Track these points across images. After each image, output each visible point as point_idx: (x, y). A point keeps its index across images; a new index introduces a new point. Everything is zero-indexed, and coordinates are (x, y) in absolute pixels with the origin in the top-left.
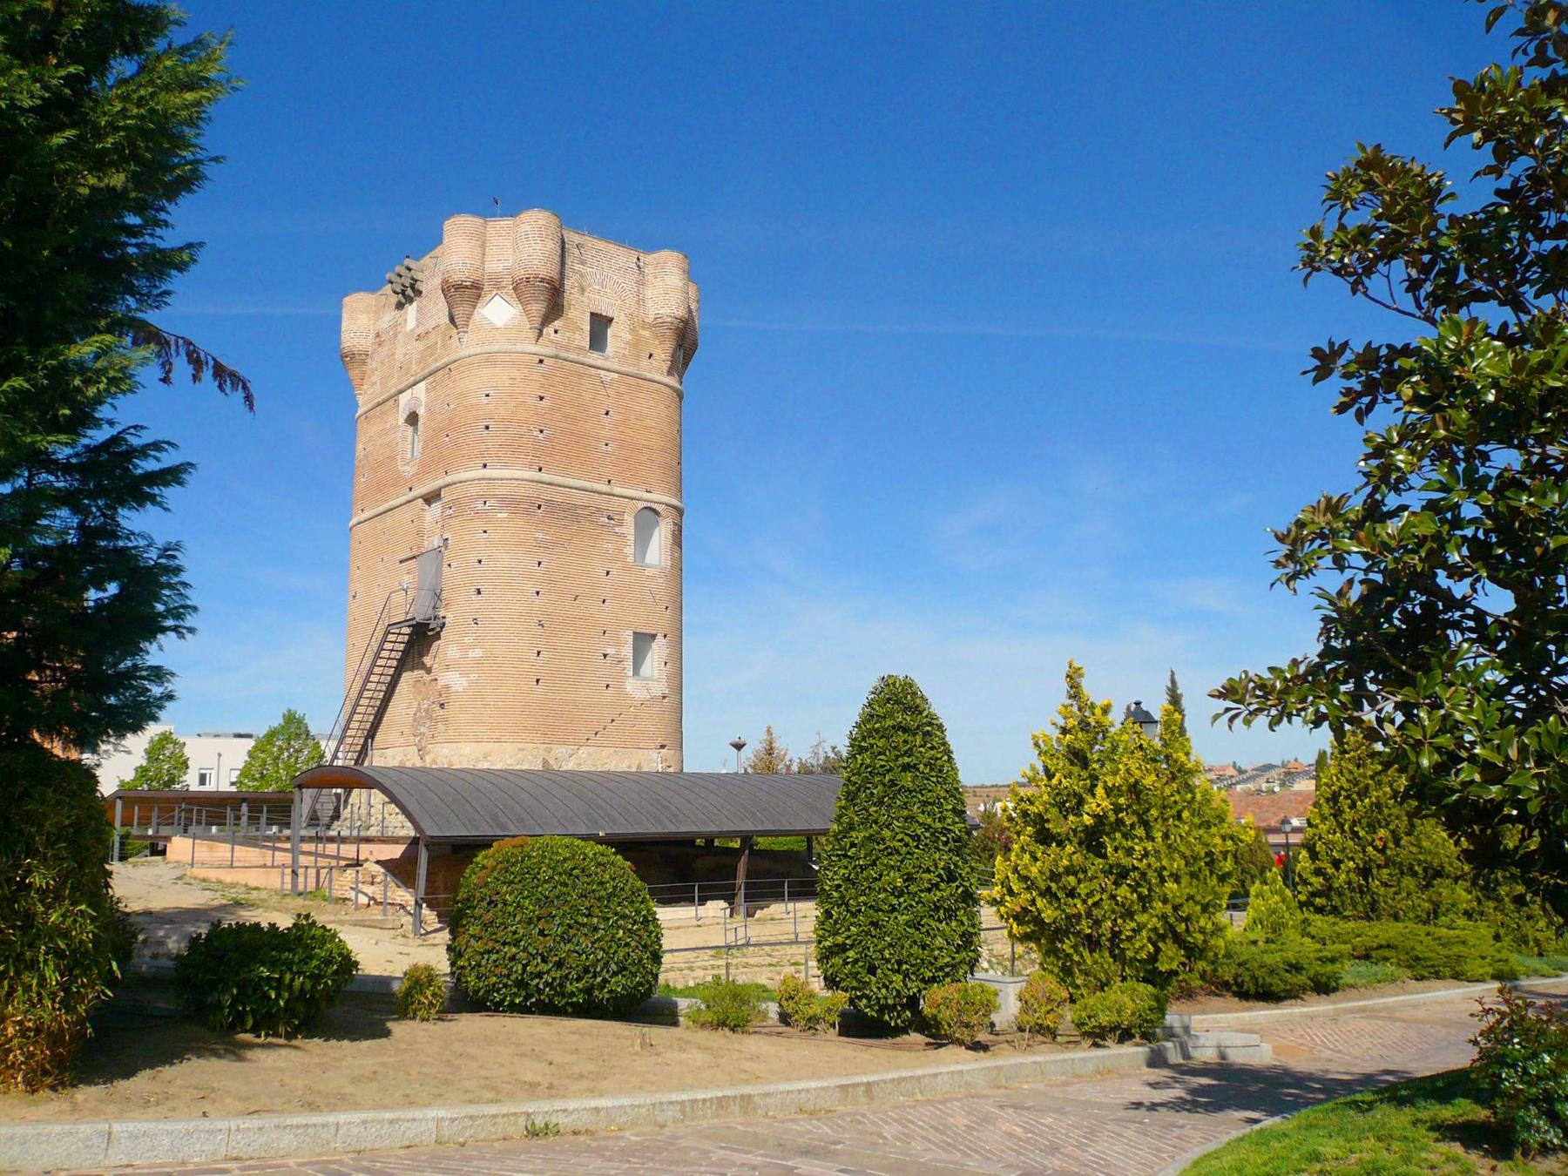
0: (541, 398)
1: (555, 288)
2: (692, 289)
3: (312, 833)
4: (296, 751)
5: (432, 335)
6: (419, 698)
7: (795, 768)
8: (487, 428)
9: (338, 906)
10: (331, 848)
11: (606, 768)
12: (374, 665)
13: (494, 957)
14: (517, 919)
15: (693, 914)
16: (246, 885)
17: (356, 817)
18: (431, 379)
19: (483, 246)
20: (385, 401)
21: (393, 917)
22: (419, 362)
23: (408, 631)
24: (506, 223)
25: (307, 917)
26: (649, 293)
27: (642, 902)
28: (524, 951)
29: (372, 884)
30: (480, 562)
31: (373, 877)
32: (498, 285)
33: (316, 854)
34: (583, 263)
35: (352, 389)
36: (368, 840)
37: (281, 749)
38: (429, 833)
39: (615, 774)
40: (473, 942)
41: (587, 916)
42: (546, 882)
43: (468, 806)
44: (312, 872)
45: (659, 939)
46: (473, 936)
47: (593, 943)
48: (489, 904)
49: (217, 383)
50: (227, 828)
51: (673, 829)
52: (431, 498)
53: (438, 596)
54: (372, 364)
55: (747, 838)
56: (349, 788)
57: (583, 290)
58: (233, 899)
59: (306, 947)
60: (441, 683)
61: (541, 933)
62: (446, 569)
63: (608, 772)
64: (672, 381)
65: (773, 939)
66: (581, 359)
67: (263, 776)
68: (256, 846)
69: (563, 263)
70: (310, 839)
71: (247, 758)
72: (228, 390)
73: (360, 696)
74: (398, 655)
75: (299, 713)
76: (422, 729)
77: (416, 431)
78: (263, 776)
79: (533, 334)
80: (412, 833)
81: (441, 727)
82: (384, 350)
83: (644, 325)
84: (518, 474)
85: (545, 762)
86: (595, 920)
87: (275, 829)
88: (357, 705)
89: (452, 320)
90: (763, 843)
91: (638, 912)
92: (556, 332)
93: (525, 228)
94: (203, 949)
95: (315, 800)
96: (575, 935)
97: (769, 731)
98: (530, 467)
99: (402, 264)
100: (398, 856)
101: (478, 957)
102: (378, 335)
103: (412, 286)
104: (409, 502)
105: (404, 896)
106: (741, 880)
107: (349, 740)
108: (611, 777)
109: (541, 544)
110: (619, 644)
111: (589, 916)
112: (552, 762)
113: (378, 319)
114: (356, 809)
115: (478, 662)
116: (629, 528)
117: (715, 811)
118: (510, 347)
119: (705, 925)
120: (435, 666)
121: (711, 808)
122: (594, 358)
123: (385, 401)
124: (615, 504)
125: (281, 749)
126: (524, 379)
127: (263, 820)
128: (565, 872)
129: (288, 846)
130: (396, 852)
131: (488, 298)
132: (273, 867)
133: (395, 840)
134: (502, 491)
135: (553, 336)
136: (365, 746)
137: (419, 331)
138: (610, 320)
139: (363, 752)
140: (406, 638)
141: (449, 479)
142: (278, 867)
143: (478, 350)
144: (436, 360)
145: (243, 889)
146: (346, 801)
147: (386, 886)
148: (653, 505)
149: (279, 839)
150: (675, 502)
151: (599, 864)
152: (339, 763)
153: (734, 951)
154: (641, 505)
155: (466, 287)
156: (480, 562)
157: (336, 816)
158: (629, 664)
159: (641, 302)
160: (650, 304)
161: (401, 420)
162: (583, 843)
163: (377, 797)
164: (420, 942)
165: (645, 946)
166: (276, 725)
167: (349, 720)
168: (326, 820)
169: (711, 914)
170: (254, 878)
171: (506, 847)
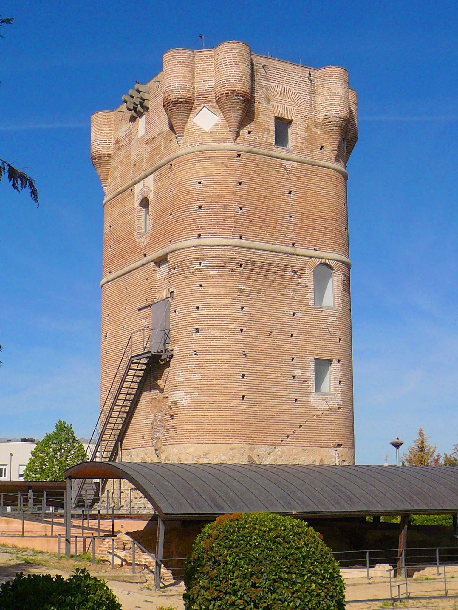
0: (240, 184)
1: (248, 100)
2: (352, 95)
3: (80, 512)
4: (66, 452)
5: (157, 140)
6: (155, 411)
7: (442, 462)
8: (200, 207)
9: (100, 566)
10: (94, 523)
11: (296, 462)
12: (121, 387)
13: (219, 603)
14: (235, 575)
15: (365, 574)
16: (33, 550)
17: (111, 500)
18: (157, 173)
19: (193, 71)
20: (124, 191)
21: (139, 574)
22: (148, 160)
23: (145, 361)
24: (208, 53)
25: (83, 571)
26: (319, 100)
27: (329, 563)
28: (241, 599)
29: (124, 549)
30: (198, 308)
31: (124, 544)
32: (205, 101)
33: (83, 528)
34: (268, 79)
35: (100, 182)
36: (120, 517)
37: (55, 450)
38: (165, 512)
39: (303, 466)
40: (202, 591)
41: (287, 573)
42: (256, 547)
43: (194, 491)
44: (80, 540)
45: (343, 592)
46: (203, 587)
47: (293, 593)
48: (214, 563)
49: (11, 183)
50: (19, 507)
51: (348, 509)
52: (160, 261)
53: (167, 335)
54: (114, 163)
55: (406, 516)
56: (105, 478)
57: (268, 100)
58: (24, 560)
59: (83, 593)
60: (171, 400)
61: (254, 585)
62: (172, 314)
63: (298, 466)
64: (339, 166)
65: (428, 594)
66: (270, 152)
67: (42, 470)
68: (39, 521)
69: (253, 80)
70: (78, 517)
71: (31, 457)
72: (19, 188)
73: (112, 410)
74: (139, 380)
75: (68, 423)
76: (158, 434)
77: (147, 212)
78: (42, 470)
80: (152, 512)
81: (172, 432)
82: (122, 153)
83: (317, 125)
85: (250, 458)
86: (294, 576)
87: (51, 509)
88: (109, 416)
89: (171, 127)
90: (418, 519)
91: (326, 571)
92: (249, 133)
93: (224, 55)
94: (12, 593)
95: (81, 488)
96: (279, 587)
97: (421, 434)
98: (234, 236)
99: (133, 88)
100: (142, 528)
101: (207, 603)
102: (117, 142)
103: (141, 104)
104: (144, 265)
105: (148, 559)
106: (402, 548)
107: (104, 443)
108: (300, 469)
109: (242, 293)
110: (304, 368)
111: (289, 573)
112: (255, 458)
113: (117, 129)
114: (110, 494)
115: (199, 383)
116: (309, 280)
117: (381, 495)
118: (215, 146)
119: (374, 583)
120: (166, 387)
121: (377, 492)
122: (279, 151)
123: (124, 191)
124: (297, 262)
125: (55, 450)
126: (226, 171)
127: (44, 502)
128: (270, 540)
129: (62, 521)
130: (140, 526)
131: (198, 110)
132: (52, 536)
133: (140, 517)
135: (247, 136)
136: (116, 447)
137: (147, 137)
138: (290, 122)
139: (115, 452)
140: (145, 366)
141: (173, 247)
142: (56, 536)
143: (191, 149)
144: (161, 159)
145: (32, 552)
146: (103, 488)
147: (134, 551)
149: (56, 516)
150: (344, 258)
151: (296, 534)
152: (97, 460)
153: (398, 603)
154: (318, 261)
155: (181, 102)
156: (198, 308)
157: (96, 499)
158: (312, 383)
159: (313, 106)
160: (319, 108)
161: (137, 204)
162: (283, 518)
163: (126, 485)
164: (161, 594)
165: (332, 597)
166: (51, 432)
167: (105, 428)
168: (89, 502)
169: (379, 574)
170: (38, 545)
171: (226, 521)
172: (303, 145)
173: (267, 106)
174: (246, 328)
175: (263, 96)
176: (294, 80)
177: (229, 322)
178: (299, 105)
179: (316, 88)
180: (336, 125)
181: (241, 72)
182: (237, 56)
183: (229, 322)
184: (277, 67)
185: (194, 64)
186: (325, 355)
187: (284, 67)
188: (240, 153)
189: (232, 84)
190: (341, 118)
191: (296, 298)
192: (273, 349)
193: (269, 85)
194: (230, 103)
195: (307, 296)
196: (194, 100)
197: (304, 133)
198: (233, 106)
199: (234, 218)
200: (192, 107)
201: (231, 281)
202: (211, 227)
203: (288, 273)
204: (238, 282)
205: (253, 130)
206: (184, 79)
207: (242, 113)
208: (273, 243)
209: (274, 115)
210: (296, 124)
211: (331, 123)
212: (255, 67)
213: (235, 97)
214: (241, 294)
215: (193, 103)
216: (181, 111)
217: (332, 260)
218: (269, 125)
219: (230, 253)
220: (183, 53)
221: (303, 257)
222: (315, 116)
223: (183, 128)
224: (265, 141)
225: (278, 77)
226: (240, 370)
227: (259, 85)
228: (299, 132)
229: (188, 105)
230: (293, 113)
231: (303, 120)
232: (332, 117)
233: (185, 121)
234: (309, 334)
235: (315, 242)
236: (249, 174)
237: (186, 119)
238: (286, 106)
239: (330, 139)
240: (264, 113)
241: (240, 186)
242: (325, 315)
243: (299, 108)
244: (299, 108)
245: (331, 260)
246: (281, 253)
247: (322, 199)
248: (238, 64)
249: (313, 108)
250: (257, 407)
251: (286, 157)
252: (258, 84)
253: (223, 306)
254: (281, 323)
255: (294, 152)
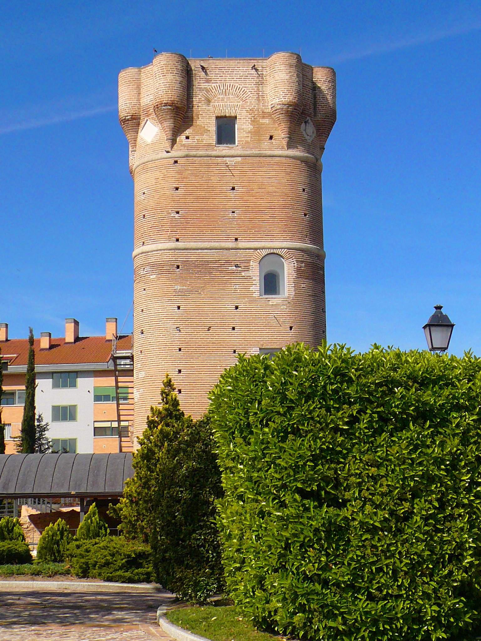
0: (177, 189)
19: (139, 88)
34: (208, 81)
57: (208, 101)
79: (167, 145)
83: (264, 115)
84: (160, 246)
92: (187, 138)
98: (169, 239)
122: (223, 149)
126: (164, 178)
134: (152, 260)
135: (185, 141)
148: (275, 251)
155: (128, 120)
159: (260, 97)
172: (249, 139)
173: (207, 108)
174: (182, 326)
175: (203, 99)
176: (239, 75)
177: (165, 322)
178: (244, 100)
179: (264, 78)
180: (282, 112)
181: (168, 82)
182: (164, 68)
183: (165, 322)
184: (218, 67)
185: (140, 81)
186: (272, 344)
187: (227, 65)
188: (176, 159)
189: (160, 96)
190: (285, 105)
191: (238, 292)
192: (212, 343)
193: (209, 87)
194: (161, 114)
195: (251, 288)
196: (140, 115)
197: (250, 126)
198: (164, 116)
199: (170, 223)
200: (139, 122)
201: (167, 282)
202: (151, 234)
203: (230, 268)
204: (174, 283)
205: (190, 134)
206: (129, 98)
207: (174, 121)
208: (213, 241)
209: (215, 115)
210: (241, 119)
211: (277, 111)
212: (194, 72)
213: (163, 107)
214: (177, 294)
215: (140, 118)
216: (130, 128)
217: (282, 249)
218: (210, 126)
219: (167, 257)
220: (128, 72)
221: (247, 251)
222: (263, 107)
223: (135, 143)
224: (204, 143)
225: (220, 76)
226: (176, 366)
227: (198, 89)
228: (244, 127)
229: (134, 121)
230: (237, 109)
231: (248, 113)
232: (276, 106)
233: (135, 136)
234: (253, 325)
235: (261, 233)
236: (186, 178)
237: (136, 135)
238: (228, 103)
239: (280, 127)
240: (204, 115)
241: (177, 191)
242: (272, 305)
243: (244, 103)
244: (244, 103)
245: (280, 249)
246: (221, 249)
247: (271, 189)
248: (165, 76)
249: (260, 99)
250: (194, 399)
251: (228, 154)
252: (197, 88)
253: (160, 307)
254: (222, 317)
255: (238, 148)
